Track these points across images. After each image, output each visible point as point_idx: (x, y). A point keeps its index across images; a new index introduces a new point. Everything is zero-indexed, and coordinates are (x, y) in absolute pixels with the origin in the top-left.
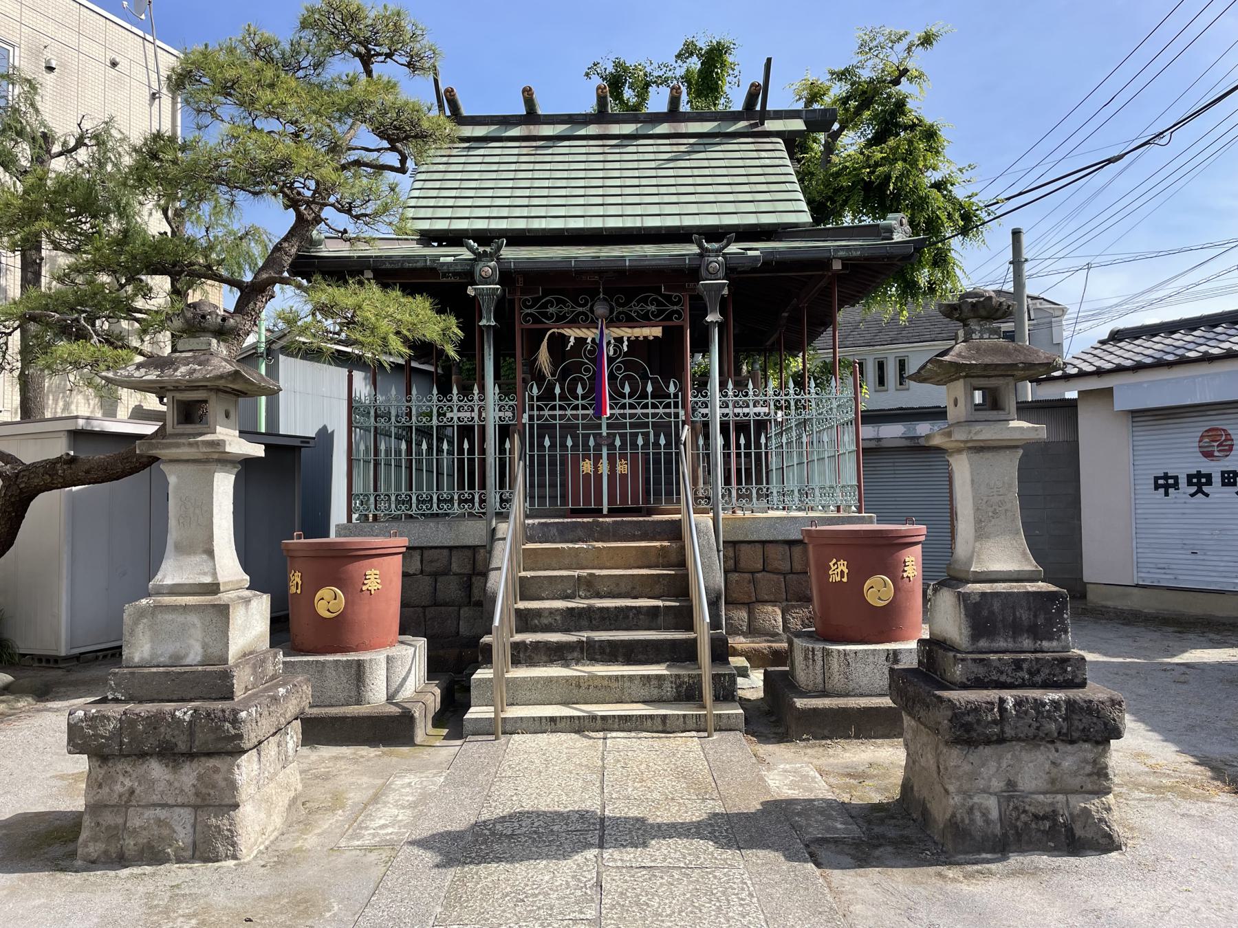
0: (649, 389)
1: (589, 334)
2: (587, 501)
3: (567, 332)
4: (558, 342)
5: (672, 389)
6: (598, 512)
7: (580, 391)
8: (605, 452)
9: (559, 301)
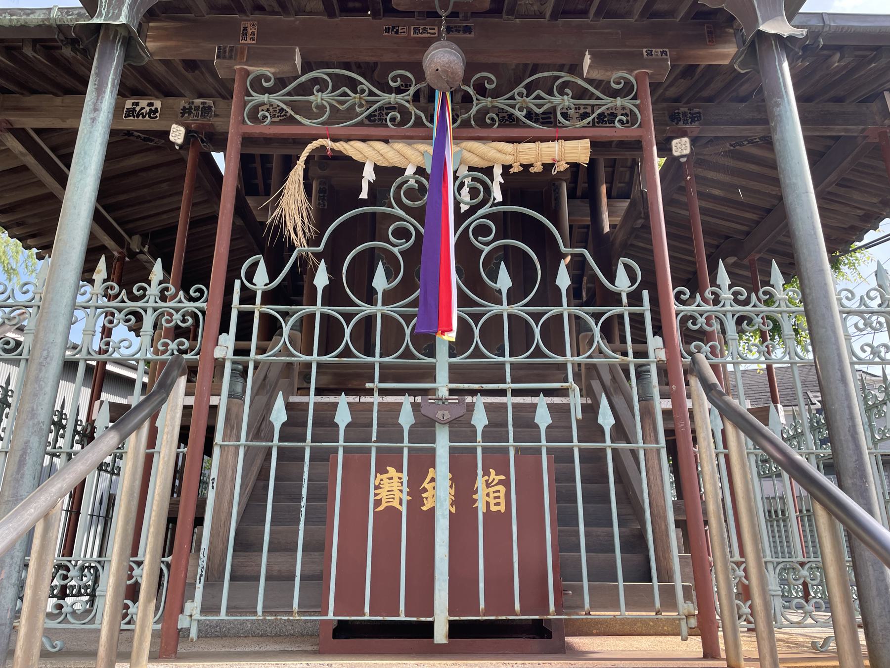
0: (563, 280)
1: (410, 156)
2: (385, 594)
3: (353, 149)
4: (334, 183)
5: (622, 283)
6: (291, 613)
7: (380, 282)
8: (443, 445)
9: (339, 81)
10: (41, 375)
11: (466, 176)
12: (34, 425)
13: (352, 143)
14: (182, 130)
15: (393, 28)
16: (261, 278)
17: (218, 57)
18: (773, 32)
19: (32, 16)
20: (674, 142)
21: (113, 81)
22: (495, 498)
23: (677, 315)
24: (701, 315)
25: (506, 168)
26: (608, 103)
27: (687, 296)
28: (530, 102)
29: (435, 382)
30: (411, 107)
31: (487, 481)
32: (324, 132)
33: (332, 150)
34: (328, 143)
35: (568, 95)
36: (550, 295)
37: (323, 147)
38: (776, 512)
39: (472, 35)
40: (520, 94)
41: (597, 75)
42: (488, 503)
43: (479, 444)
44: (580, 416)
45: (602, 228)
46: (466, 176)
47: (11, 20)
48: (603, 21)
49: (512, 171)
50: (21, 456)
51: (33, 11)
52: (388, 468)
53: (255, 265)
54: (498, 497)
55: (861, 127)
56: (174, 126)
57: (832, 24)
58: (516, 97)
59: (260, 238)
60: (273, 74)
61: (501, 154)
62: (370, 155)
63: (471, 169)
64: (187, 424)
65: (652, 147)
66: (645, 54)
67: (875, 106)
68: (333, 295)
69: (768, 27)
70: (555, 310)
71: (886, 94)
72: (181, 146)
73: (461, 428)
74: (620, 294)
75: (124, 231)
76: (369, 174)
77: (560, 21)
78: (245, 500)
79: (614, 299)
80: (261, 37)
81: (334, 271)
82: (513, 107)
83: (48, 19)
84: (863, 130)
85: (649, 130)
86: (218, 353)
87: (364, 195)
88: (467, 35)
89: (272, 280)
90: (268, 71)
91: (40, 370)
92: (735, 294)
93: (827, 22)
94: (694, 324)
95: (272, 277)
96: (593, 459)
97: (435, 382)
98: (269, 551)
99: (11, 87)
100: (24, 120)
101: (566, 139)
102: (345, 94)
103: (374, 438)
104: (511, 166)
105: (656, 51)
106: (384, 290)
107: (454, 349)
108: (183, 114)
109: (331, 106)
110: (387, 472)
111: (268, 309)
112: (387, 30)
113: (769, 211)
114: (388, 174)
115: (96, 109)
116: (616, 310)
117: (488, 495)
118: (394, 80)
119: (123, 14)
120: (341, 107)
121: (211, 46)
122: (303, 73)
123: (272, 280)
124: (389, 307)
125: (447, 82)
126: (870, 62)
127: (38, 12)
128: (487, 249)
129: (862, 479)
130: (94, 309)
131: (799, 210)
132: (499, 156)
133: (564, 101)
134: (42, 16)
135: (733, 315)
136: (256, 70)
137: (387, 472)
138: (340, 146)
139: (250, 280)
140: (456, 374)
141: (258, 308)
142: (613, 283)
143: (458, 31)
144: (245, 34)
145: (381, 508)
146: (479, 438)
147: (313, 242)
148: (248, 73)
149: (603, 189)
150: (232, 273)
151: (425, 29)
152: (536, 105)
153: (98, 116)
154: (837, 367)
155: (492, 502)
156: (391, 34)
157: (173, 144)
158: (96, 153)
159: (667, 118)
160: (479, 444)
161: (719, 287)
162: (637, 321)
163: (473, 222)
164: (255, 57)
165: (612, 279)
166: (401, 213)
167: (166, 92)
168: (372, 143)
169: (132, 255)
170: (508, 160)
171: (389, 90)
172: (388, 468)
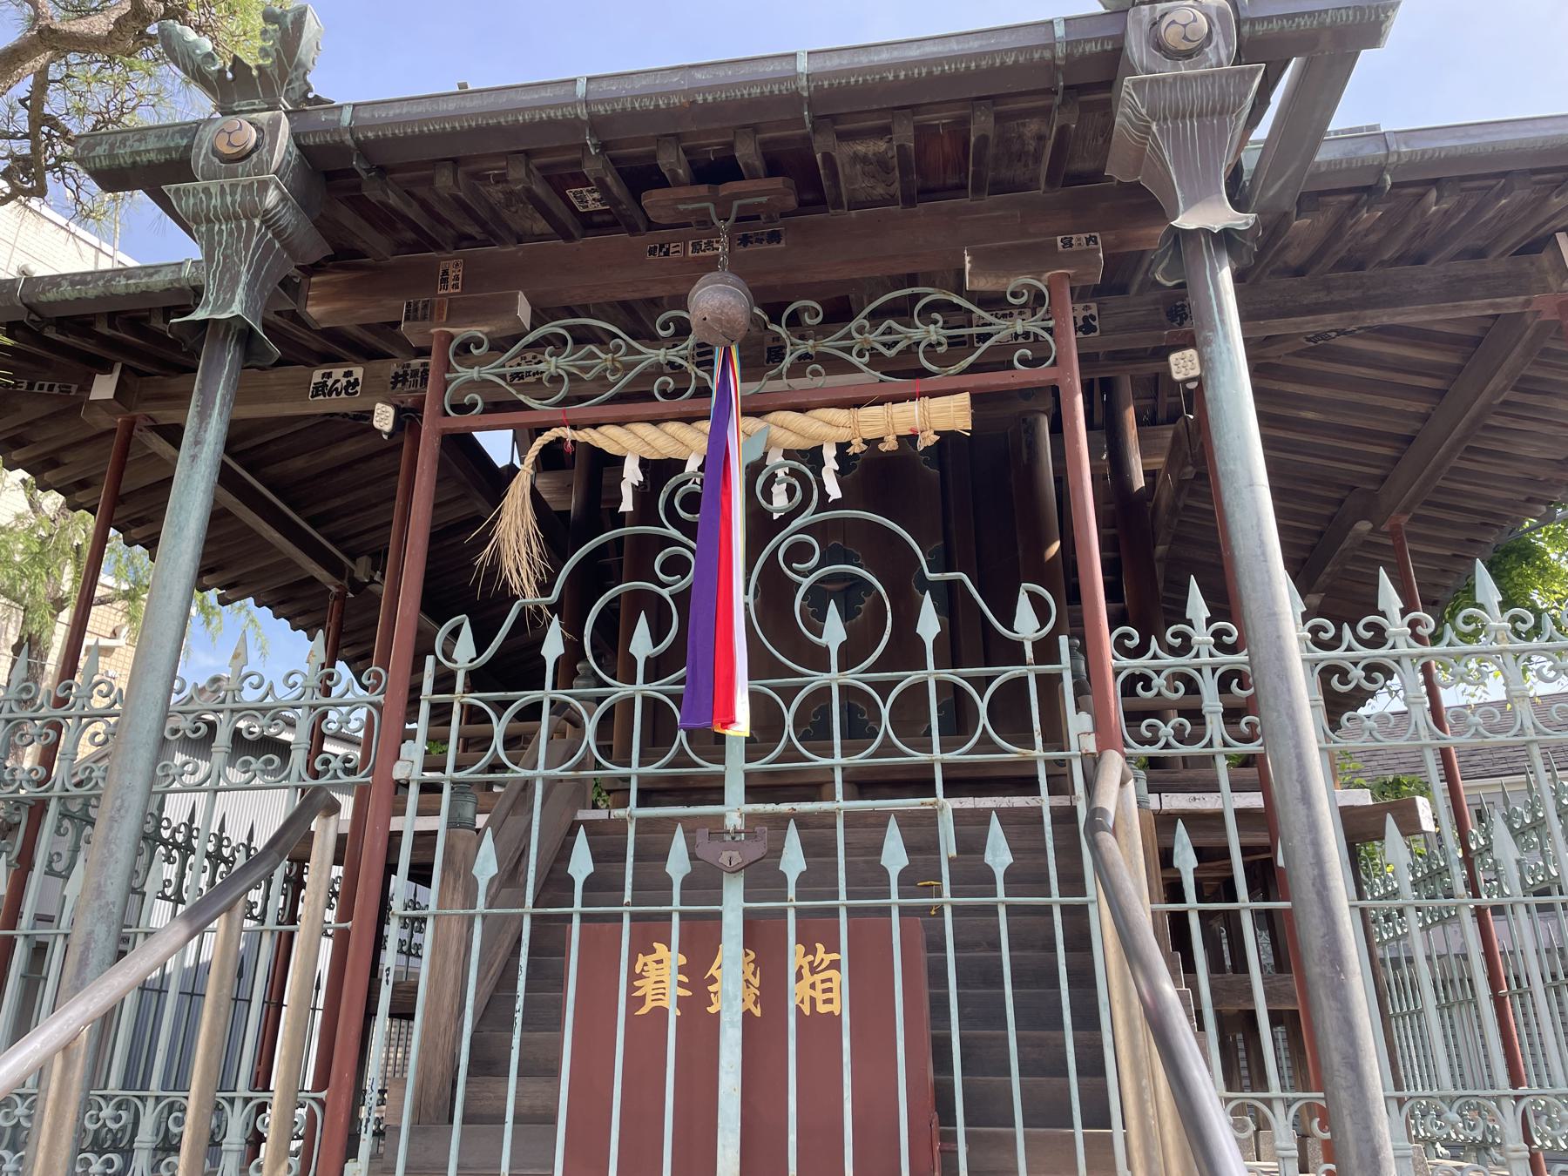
0: (929, 625)
3: (608, 439)
5: (1026, 626)
7: (641, 645)
8: (733, 905)
9: (583, 337)
10: (112, 835)
11: (780, 466)
12: (101, 908)
13: (603, 429)
14: (391, 411)
15: (662, 246)
16: (465, 649)
17: (407, 318)
18: (1193, 227)
19: (156, 278)
20: (1173, 358)
21: (223, 397)
22: (824, 991)
23: (1117, 674)
24: (1158, 673)
25: (842, 447)
26: (1004, 329)
27: (1137, 641)
28: (874, 338)
29: (722, 802)
30: (691, 368)
31: (811, 963)
32: (561, 417)
33: (574, 442)
34: (567, 433)
35: (935, 322)
36: (906, 651)
37: (560, 440)
38: (1517, 978)
39: (782, 245)
40: (861, 330)
41: (984, 284)
42: (813, 1000)
43: (792, 903)
44: (953, 853)
45: (1131, 486)
46: (780, 466)
47: (127, 286)
48: (989, 200)
49: (851, 451)
50: (83, 953)
51: (157, 269)
52: (655, 945)
53: (455, 633)
54: (830, 990)
55: (1521, 299)
56: (379, 405)
57: (1403, 149)
58: (855, 334)
59: (460, 587)
60: (486, 334)
61: (830, 428)
62: (633, 443)
63: (788, 454)
64: (425, 860)
65: (1073, 396)
66: (1060, 244)
67: (1545, 258)
68: (568, 670)
69: (1186, 221)
70: (914, 676)
71: (1561, 237)
72: (391, 435)
73: (763, 878)
74: (1021, 644)
75: (343, 552)
76: (632, 474)
77: (921, 207)
78: (488, 988)
79: (1014, 653)
80: (471, 279)
81: (573, 628)
82: (848, 350)
83: (178, 280)
84: (1528, 303)
85: (1071, 369)
86: (399, 772)
87: (627, 505)
88: (775, 246)
89: (479, 653)
90: (477, 331)
91: (111, 828)
92: (1217, 634)
93: (1394, 148)
94: (1147, 688)
95: (480, 647)
96: (975, 923)
97: (722, 802)
98: (519, 1075)
99: (148, 369)
100: (171, 413)
101: (933, 395)
102: (592, 355)
103: (628, 898)
104: (849, 444)
105: (1079, 239)
106: (648, 658)
107: (754, 748)
108: (394, 384)
109: (569, 374)
110: (654, 951)
111: (473, 699)
112: (652, 251)
113: (1409, 440)
114: (659, 470)
115: (197, 442)
116: (1015, 671)
117: (813, 986)
118: (665, 327)
119: (237, 298)
120: (586, 377)
121: (396, 303)
122: (533, 328)
123: (479, 653)
124: (654, 686)
125: (724, 334)
126: (1498, 197)
127: (164, 270)
128: (806, 583)
129: (1333, 966)
130: (228, 714)
131: (1238, 516)
132: (826, 430)
133: (933, 333)
134: (170, 276)
135: (1214, 671)
136: (462, 332)
137: (654, 951)
138: (585, 436)
139: (448, 657)
140: (755, 791)
141: (460, 697)
142: (1011, 629)
143: (760, 241)
144: (445, 281)
145: (643, 1011)
146: (792, 893)
147: (544, 588)
148: (452, 337)
149: (1130, 415)
150: (423, 648)
151: (709, 244)
152: (884, 344)
153: (201, 451)
154: (1295, 777)
155: (820, 996)
156: (659, 255)
157: (379, 432)
158: (197, 504)
159: (1163, 317)
160: (792, 903)
161: (1190, 623)
162: (1049, 685)
163: (782, 542)
164: (461, 311)
165: (1008, 619)
166: (673, 532)
167: (369, 354)
168: (633, 426)
169: (358, 587)
170: (843, 435)
171: (652, 340)
172: (655, 945)
